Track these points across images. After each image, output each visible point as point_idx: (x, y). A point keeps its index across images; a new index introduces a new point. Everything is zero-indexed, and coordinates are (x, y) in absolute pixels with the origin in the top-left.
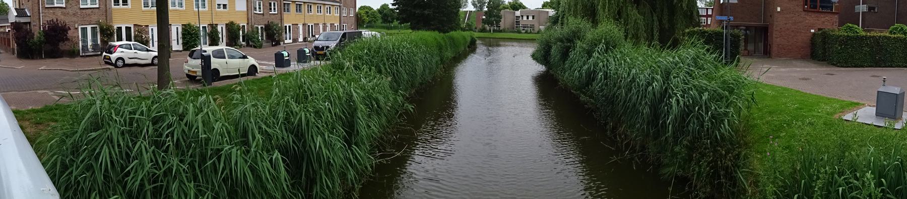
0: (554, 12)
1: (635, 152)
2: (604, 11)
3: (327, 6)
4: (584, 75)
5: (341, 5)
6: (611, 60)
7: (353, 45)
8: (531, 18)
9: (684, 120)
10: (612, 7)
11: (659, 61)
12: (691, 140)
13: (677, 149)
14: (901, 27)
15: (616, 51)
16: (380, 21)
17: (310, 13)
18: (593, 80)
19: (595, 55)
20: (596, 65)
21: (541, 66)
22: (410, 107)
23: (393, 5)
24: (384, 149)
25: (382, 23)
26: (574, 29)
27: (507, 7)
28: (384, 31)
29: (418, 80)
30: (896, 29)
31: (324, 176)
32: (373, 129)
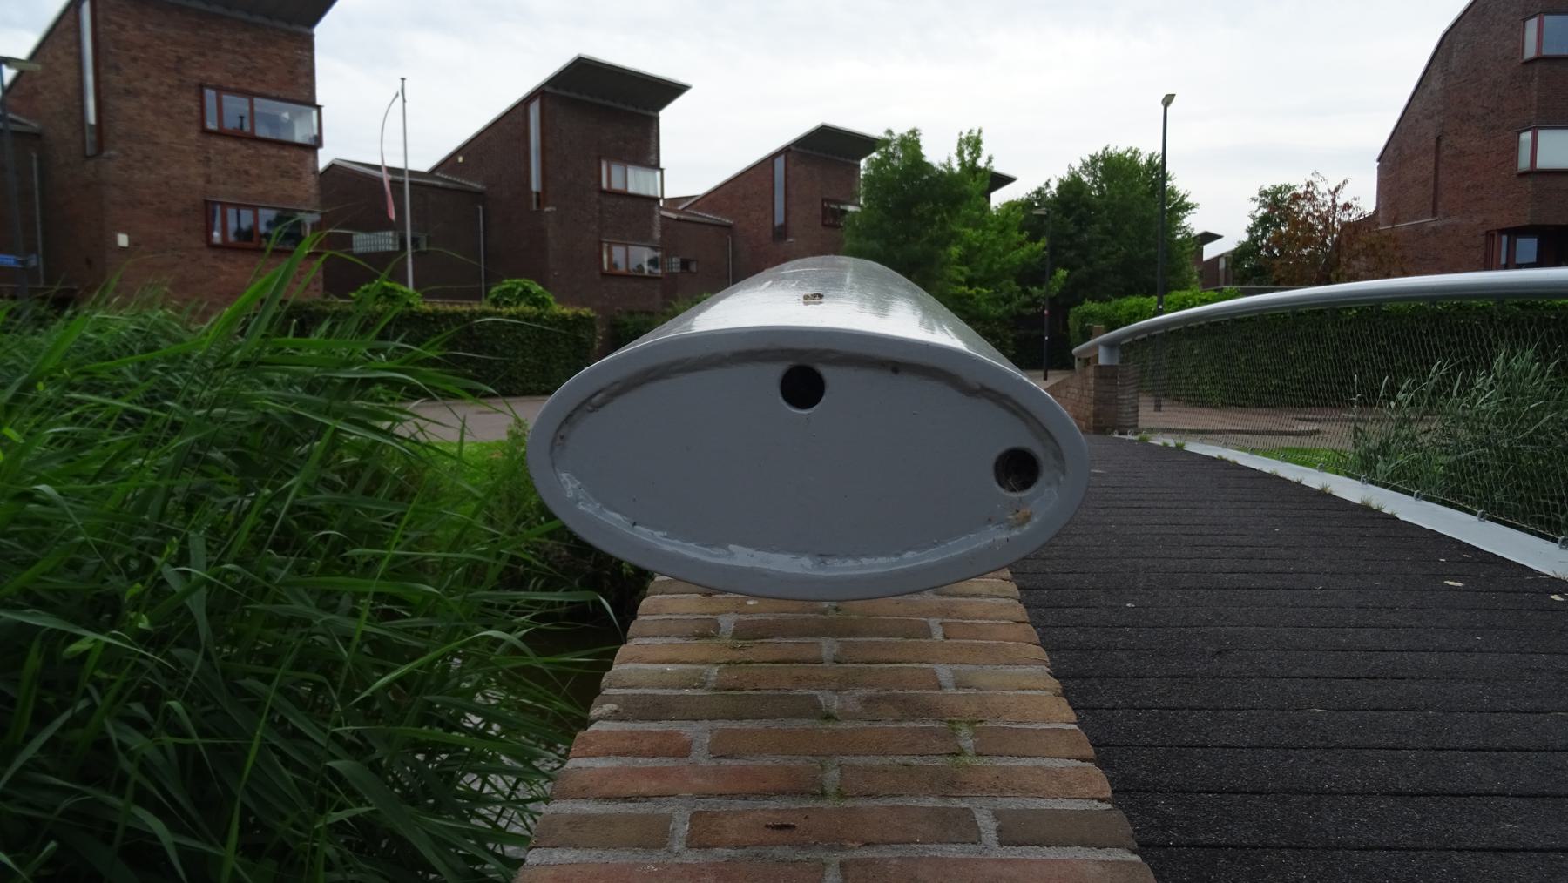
14: (523, 286)
30: (510, 292)
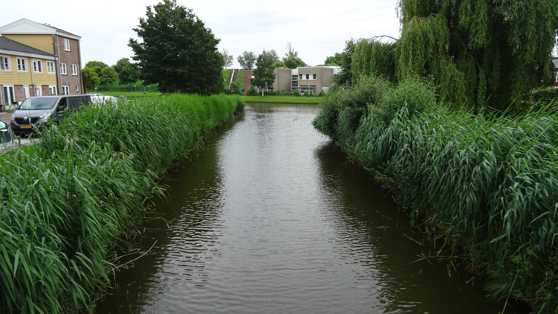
0: (340, 70)
1: (449, 252)
2: (406, 65)
3: (33, 61)
4: (380, 147)
5: (57, 59)
6: (417, 127)
7: (77, 114)
8: (311, 77)
9: (529, 217)
10: (417, 59)
11: (491, 133)
12: (541, 251)
13: (517, 259)
15: (424, 116)
16: (118, 81)
17: (6, 70)
18: (392, 153)
19: (395, 121)
20: (395, 135)
21: (324, 136)
22: (161, 190)
23: (135, 59)
24: (126, 248)
25: (120, 84)
26: (366, 89)
27: (281, 64)
28: (123, 94)
29: (173, 155)
31: (32, 305)
32: (108, 227)
